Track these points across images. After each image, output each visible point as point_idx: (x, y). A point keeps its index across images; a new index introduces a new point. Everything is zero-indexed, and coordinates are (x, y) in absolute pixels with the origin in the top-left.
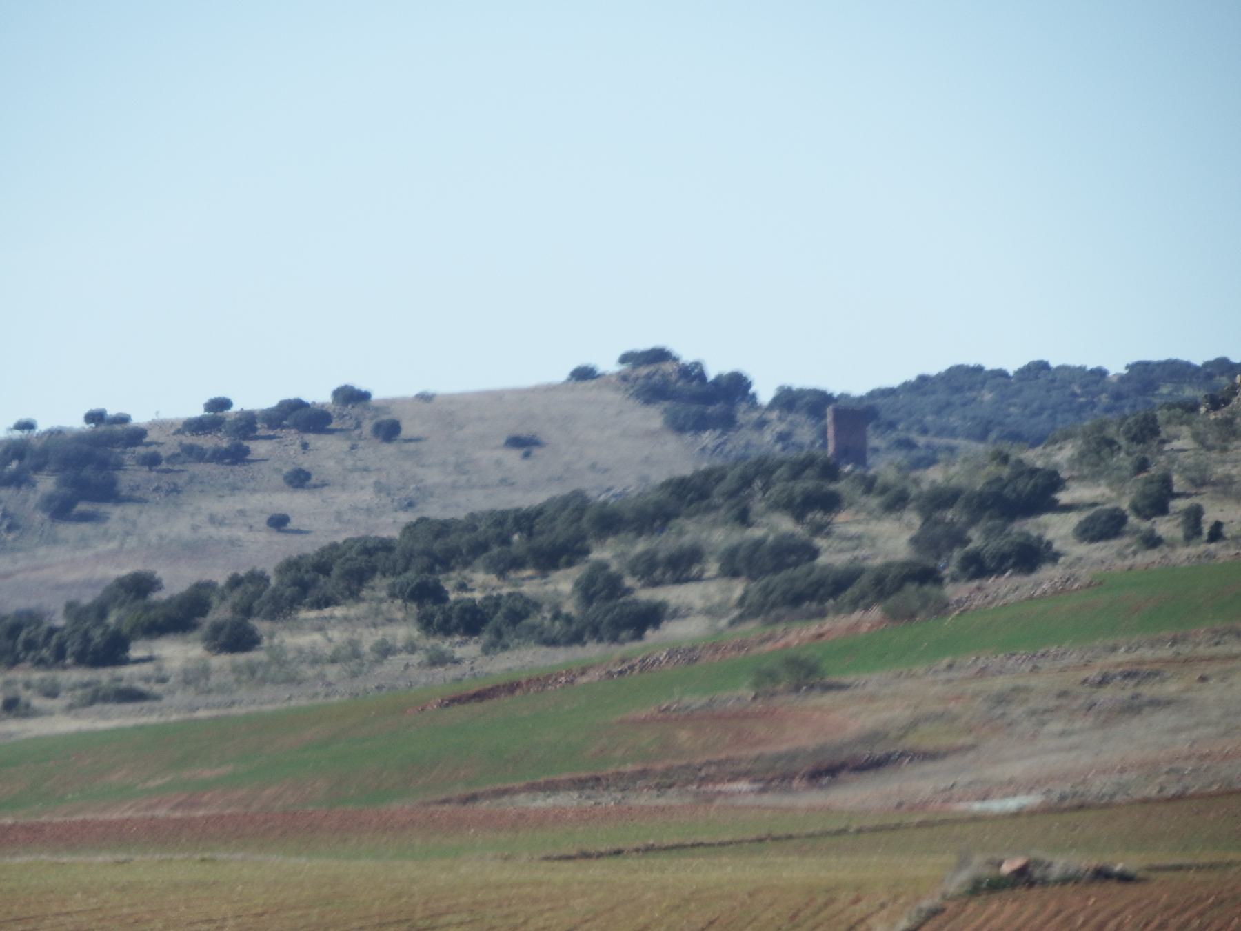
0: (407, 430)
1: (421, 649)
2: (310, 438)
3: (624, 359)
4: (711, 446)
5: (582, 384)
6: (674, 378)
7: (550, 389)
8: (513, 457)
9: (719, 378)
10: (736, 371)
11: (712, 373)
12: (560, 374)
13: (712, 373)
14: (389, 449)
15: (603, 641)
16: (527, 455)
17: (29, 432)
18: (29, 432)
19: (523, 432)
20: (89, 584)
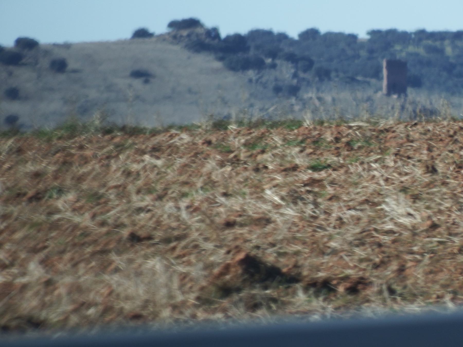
0: (72, 65)
1: (308, 253)
2: (11, 68)
3: (173, 24)
4: (254, 78)
5: (140, 40)
6: (203, 37)
7: (121, 44)
8: (138, 83)
9: (228, 38)
10: (38, 42)
11: (223, 34)
12: (127, 34)
13: (223, 34)
14: (62, 77)
15: (126, 187)
16: (146, 82)
17: (189, 58)
18: (189, 58)
19: (144, 66)
20: (292, 250)
